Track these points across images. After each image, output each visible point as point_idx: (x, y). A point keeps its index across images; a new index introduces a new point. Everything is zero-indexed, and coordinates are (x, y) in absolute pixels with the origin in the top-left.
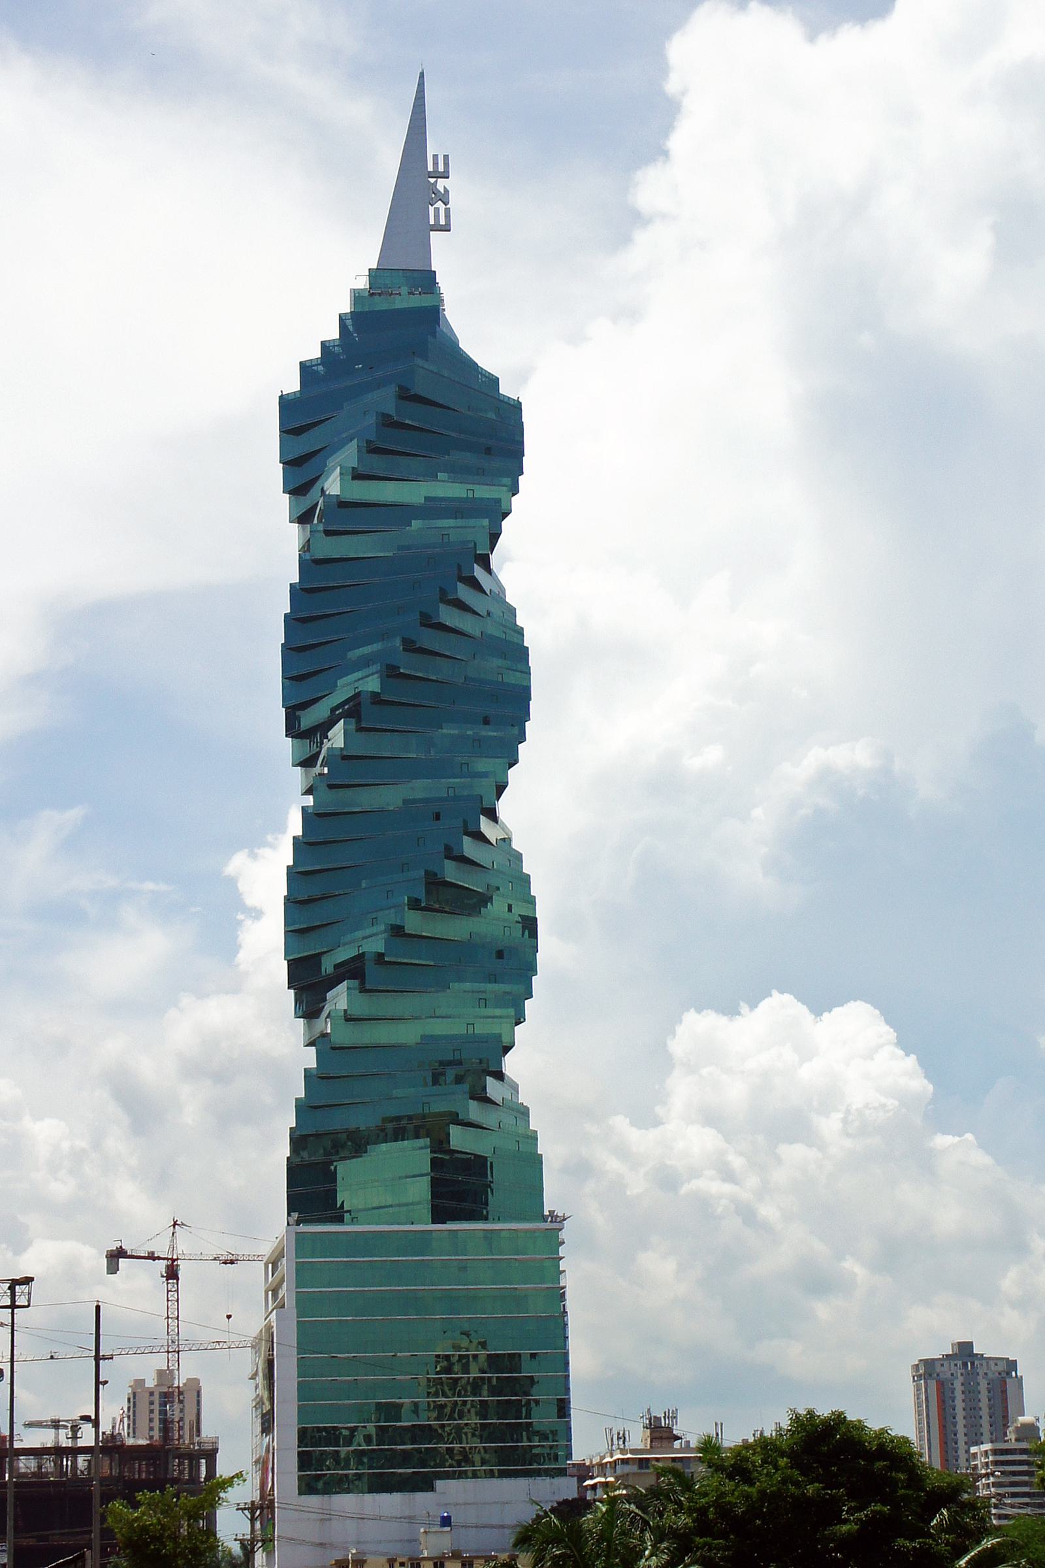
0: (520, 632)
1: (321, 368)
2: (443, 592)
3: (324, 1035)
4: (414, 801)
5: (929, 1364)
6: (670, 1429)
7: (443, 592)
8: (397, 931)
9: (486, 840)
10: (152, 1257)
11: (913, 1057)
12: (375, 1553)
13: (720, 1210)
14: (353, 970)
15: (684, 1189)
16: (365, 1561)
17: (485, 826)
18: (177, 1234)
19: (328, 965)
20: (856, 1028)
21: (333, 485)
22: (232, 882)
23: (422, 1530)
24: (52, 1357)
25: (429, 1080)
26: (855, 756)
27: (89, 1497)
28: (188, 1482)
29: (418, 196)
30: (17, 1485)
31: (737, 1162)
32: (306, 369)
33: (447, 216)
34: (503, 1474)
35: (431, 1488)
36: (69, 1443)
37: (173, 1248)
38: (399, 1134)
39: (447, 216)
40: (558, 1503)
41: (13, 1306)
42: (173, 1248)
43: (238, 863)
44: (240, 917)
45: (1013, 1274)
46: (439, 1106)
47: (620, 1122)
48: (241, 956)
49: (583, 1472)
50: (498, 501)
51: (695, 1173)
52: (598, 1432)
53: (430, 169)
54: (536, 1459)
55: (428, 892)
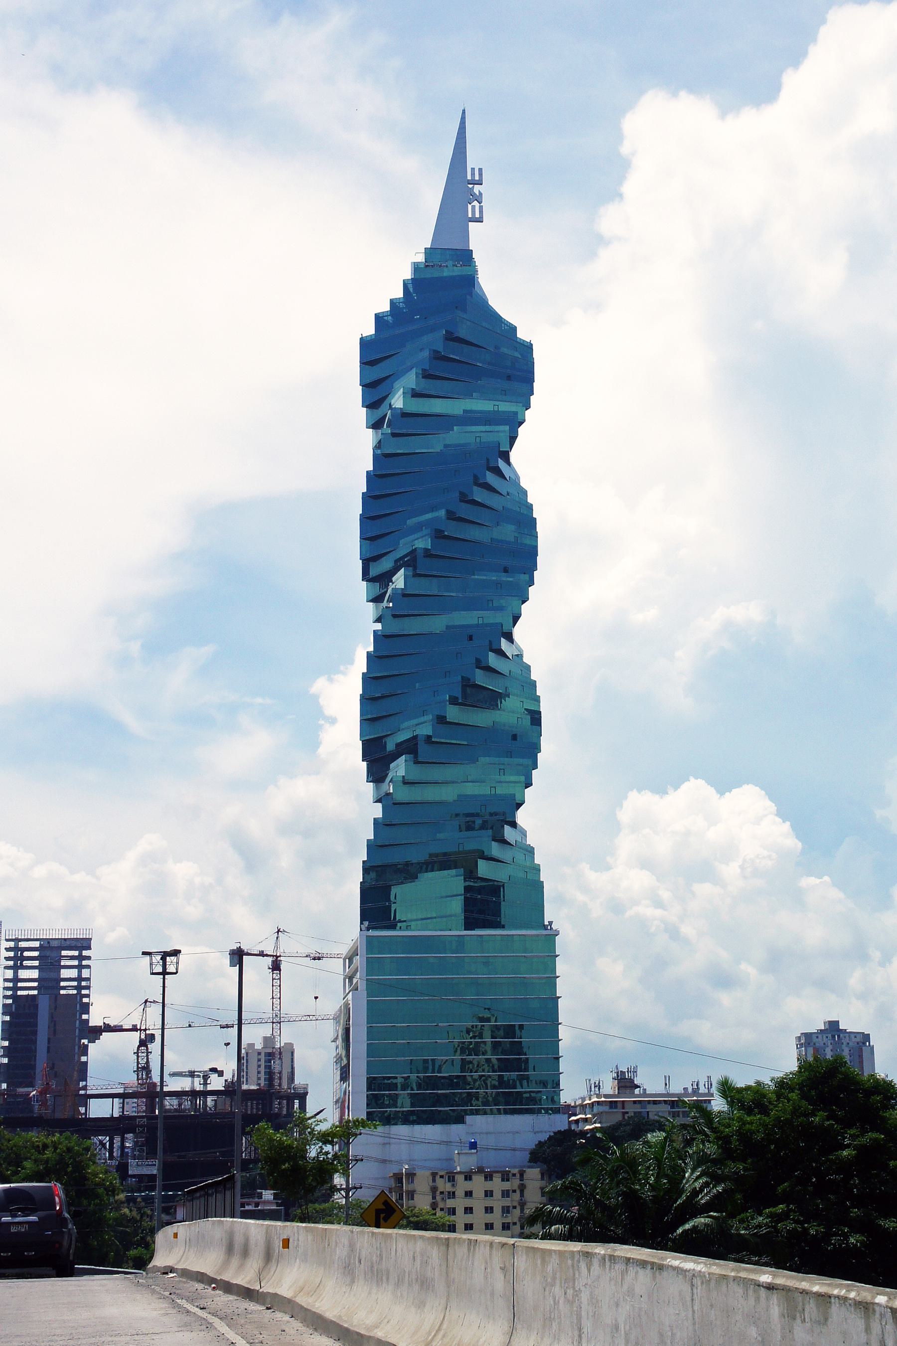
1: (390, 318)
2: (476, 477)
5: (808, 1036)
7: (476, 477)
8: (441, 720)
9: (504, 655)
10: (262, 954)
11: (788, 823)
12: (423, 1168)
13: (653, 929)
14: (410, 748)
15: (629, 913)
16: (415, 1174)
17: (504, 644)
18: (280, 938)
19: (391, 746)
20: (749, 800)
21: (398, 401)
22: (315, 698)
24: (190, 1026)
25: (463, 827)
26: (748, 613)
27: (232, 1127)
28: (285, 1116)
29: (461, 193)
30: (165, 1118)
31: (665, 895)
32: (379, 319)
33: (481, 211)
34: (506, 1112)
36: (201, 1088)
37: (277, 947)
40: (555, 1133)
41: (164, 973)
42: (277, 947)
43: (320, 684)
45: (858, 974)
46: (471, 846)
47: (585, 867)
48: (322, 751)
49: (569, 1110)
50: (516, 413)
53: (469, 178)
55: (464, 692)
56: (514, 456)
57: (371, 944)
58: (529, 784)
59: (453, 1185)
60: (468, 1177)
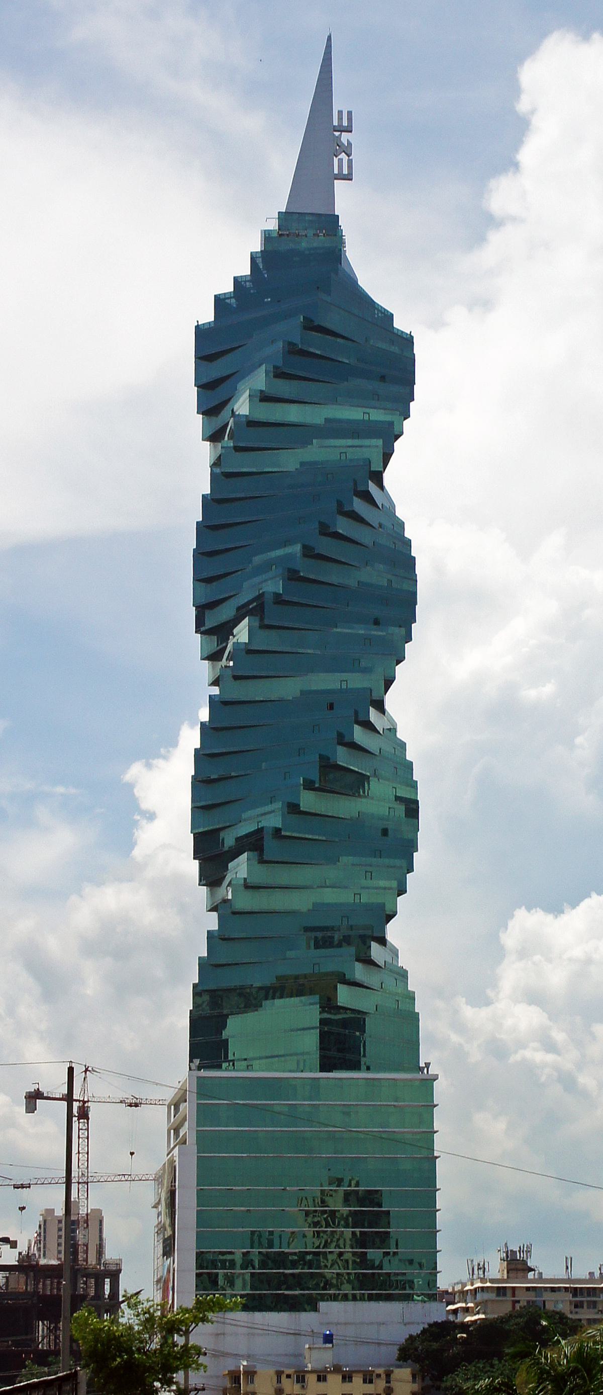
0: (408, 543)
1: (233, 301)
2: (340, 504)
3: (225, 901)
4: (310, 692)
6: (524, 1262)
8: (293, 808)
13: (543, 1079)
14: (253, 843)
16: (255, 1372)
17: (373, 715)
19: (229, 840)
21: (242, 406)
22: (130, 786)
23: (307, 1346)
28: (93, 1298)
31: (559, 1036)
33: (350, 167)
34: (371, 1298)
35: (315, 1309)
38: (299, 992)
39: (350, 167)
43: (136, 771)
44: (137, 817)
46: (329, 966)
48: (137, 852)
49: (448, 1297)
50: (391, 424)
51: (521, 1045)
52: (463, 1262)
54: (327, 1285)
56: (388, 477)
57: (204, 1089)
58: (402, 891)
59: (303, 1386)
60: (321, 1378)
